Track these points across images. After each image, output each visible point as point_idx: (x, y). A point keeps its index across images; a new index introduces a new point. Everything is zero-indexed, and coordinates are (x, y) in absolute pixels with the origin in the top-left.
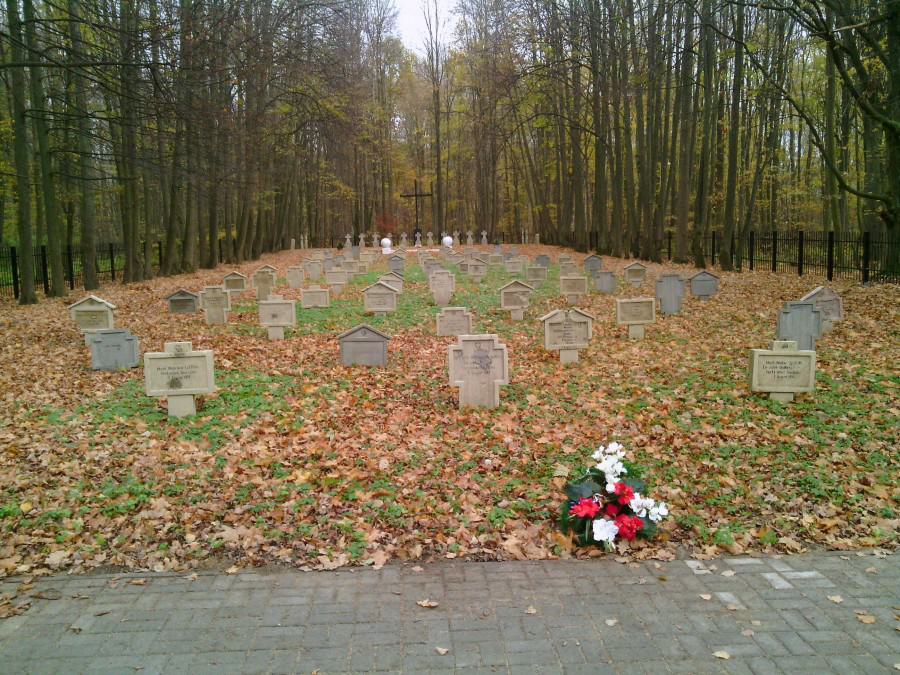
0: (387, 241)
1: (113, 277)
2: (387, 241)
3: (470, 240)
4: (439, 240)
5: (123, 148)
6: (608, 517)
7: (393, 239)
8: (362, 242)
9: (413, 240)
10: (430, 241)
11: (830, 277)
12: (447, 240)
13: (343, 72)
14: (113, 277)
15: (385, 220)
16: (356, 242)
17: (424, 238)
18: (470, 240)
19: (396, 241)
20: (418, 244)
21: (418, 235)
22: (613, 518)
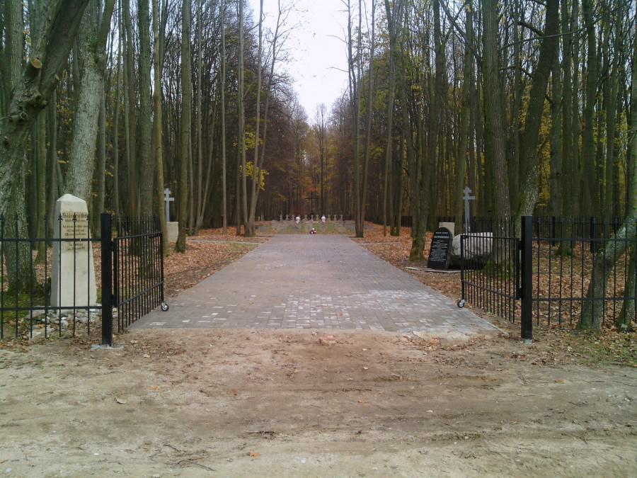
0: (298, 218)
1: (75, 216)
2: (298, 218)
3: (335, 219)
4: (320, 218)
5: (156, 463)
6: (353, 227)
7: (301, 217)
8: (287, 218)
9: (309, 218)
10: (317, 219)
11: (526, 332)
12: (324, 218)
13: (233, 84)
14: (75, 216)
15: (297, 209)
16: (284, 218)
17: (314, 218)
18: (335, 219)
19: (302, 218)
20: (312, 220)
21: (312, 216)
22: (271, 98)
